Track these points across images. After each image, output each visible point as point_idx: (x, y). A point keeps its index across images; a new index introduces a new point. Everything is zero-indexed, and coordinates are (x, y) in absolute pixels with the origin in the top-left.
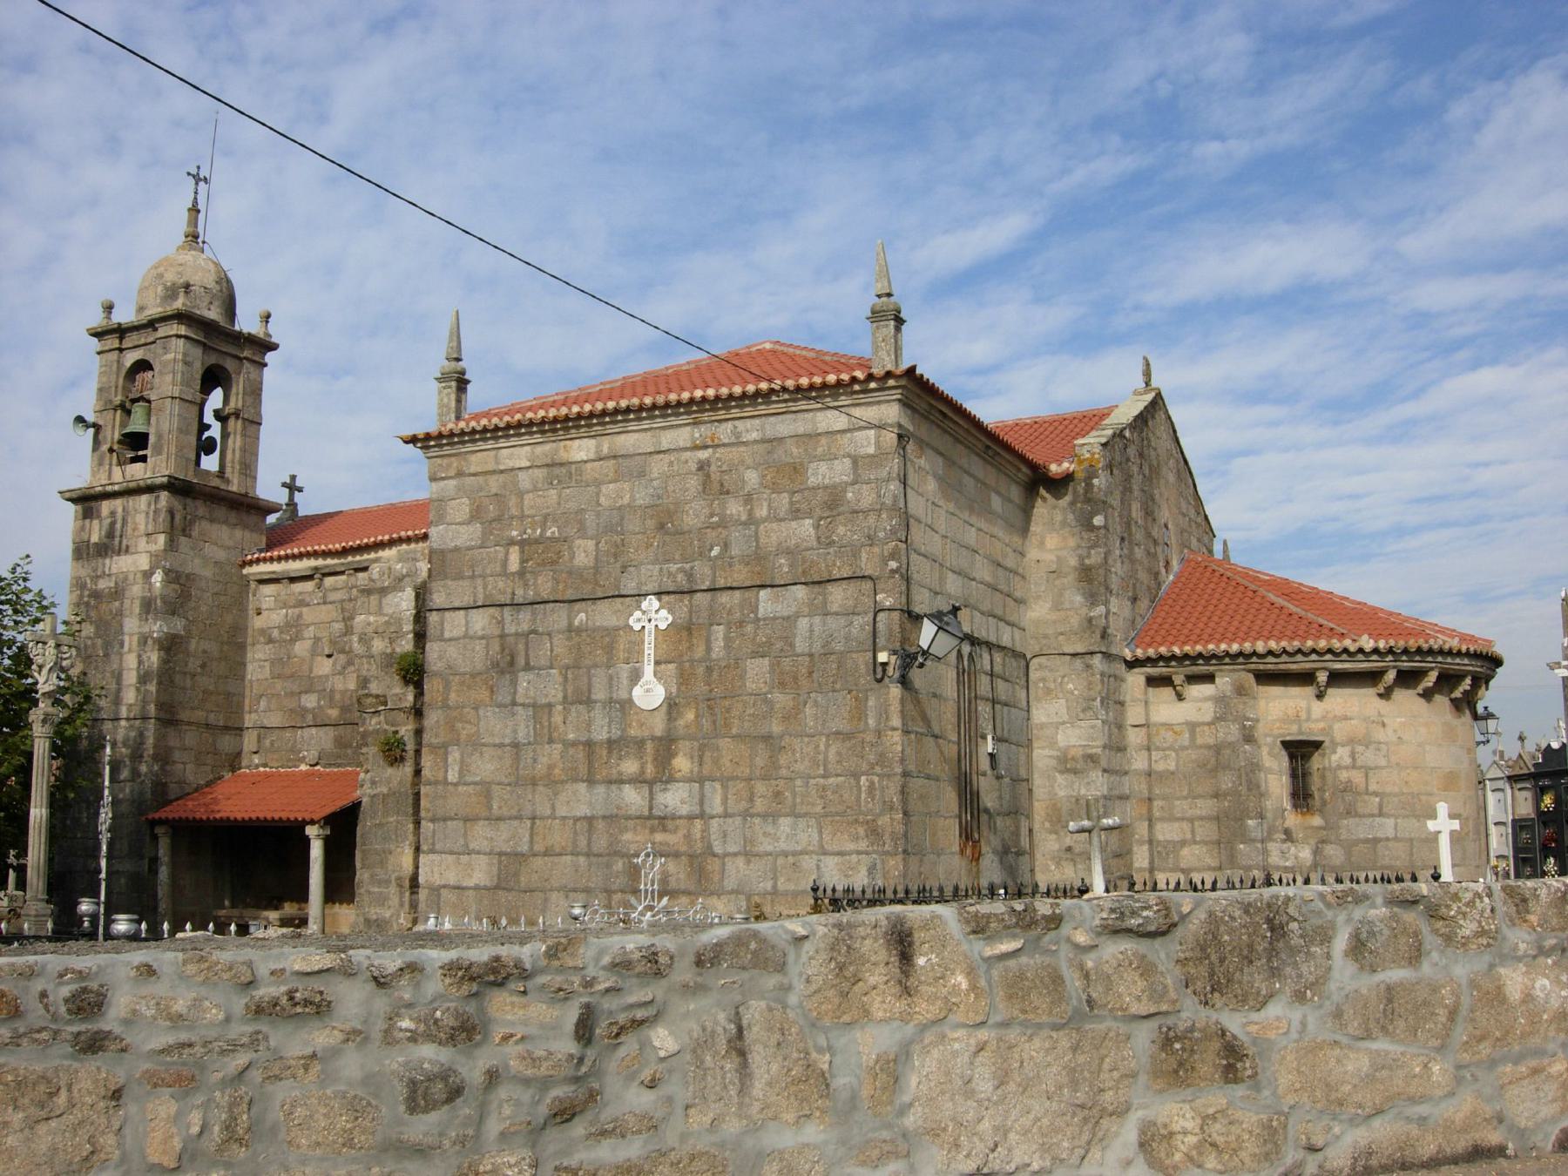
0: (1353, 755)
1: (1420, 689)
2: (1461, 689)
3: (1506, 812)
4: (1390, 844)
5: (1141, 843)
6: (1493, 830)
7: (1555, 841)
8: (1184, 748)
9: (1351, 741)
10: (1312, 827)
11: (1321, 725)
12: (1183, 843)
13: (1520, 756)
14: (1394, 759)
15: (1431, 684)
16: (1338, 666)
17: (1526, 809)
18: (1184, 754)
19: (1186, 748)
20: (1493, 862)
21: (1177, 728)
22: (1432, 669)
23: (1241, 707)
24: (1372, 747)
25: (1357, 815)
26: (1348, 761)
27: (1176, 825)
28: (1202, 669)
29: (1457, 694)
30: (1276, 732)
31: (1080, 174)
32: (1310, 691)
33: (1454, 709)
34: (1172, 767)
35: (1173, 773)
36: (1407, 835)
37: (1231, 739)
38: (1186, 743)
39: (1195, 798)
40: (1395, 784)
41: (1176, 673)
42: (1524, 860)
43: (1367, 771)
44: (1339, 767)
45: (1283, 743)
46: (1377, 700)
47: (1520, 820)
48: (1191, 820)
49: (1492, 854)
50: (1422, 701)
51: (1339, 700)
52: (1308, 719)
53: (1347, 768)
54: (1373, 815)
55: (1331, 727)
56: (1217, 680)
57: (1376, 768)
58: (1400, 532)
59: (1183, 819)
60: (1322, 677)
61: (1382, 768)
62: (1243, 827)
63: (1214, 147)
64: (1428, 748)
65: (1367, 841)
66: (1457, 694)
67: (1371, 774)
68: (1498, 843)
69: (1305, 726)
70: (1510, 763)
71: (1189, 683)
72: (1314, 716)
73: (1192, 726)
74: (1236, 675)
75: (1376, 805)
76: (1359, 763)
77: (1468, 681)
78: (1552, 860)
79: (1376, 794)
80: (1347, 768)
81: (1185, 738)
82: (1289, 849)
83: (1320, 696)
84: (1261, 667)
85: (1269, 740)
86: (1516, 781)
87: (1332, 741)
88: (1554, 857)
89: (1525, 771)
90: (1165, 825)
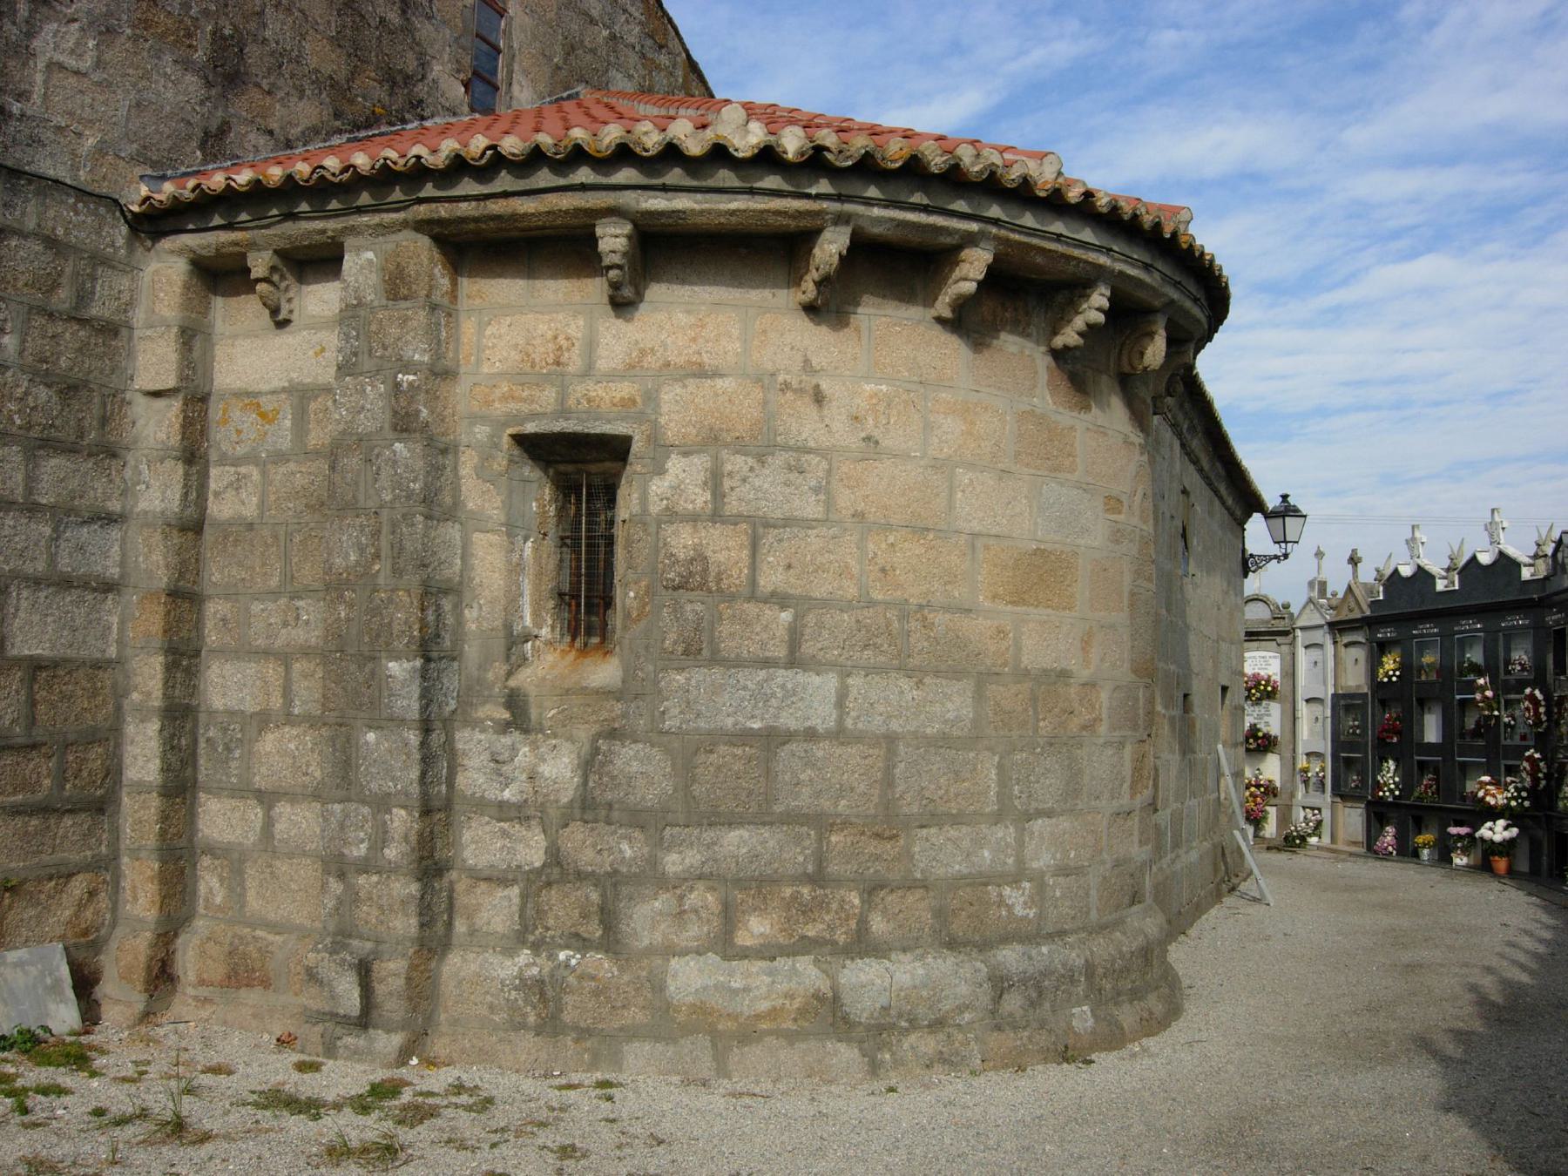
0: (715, 480)
1: (943, 307)
2: (1079, 322)
3: (1325, 683)
4: (820, 750)
5: (143, 715)
6: (1303, 710)
7: (1398, 733)
8: (280, 457)
9: (711, 441)
10: (584, 691)
11: (624, 389)
12: (263, 720)
13: (1350, 589)
14: (845, 500)
15: (969, 287)
16: (656, 203)
17: (1356, 679)
18: (279, 473)
19: (280, 457)
20: (1302, 762)
21: (267, 404)
22: (970, 240)
23: (394, 331)
24: (779, 460)
25: (716, 660)
26: (700, 499)
27: (251, 668)
28: (309, 228)
29: (1069, 336)
30: (499, 409)
31: (1037, 55)
32: (595, 289)
33: (1064, 384)
34: (250, 511)
35: (250, 526)
36: (876, 724)
37: (365, 424)
38: (286, 443)
39: (295, 596)
40: (844, 572)
41: (253, 245)
42: (1349, 762)
43: (757, 528)
44: (671, 515)
45: (520, 440)
46: (803, 323)
47: (1344, 696)
48: (285, 658)
49: (1301, 750)
50: (952, 347)
51: (681, 318)
52: (588, 372)
53: (694, 518)
54: (767, 663)
55: (651, 397)
56: (349, 262)
57: (788, 522)
58: (1322, 412)
59: (266, 653)
60: (613, 239)
61: (807, 524)
62: (376, 680)
63: (1169, 37)
64: (963, 476)
65: (743, 737)
66: (1069, 336)
67: (770, 537)
68: (1311, 732)
69: (578, 390)
70: (1334, 603)
71: (302, 279)
72: (602, 365)
73: (302, 395)
74: (389, 243)
75: (781, 632)
76: (733, 505)
77: (1099, 298)
78: (1391, 764)
79: (780, 599)
80: (694, 518)
81: (283, 434)
82: (514, 750)
83: (622, 305)
84: (443, 211)
85: (481, 432)
86: (1341, 631)
87: (655, 439)
88: (1396, 760)
89: (1357, 615)
90: (229, 668)
